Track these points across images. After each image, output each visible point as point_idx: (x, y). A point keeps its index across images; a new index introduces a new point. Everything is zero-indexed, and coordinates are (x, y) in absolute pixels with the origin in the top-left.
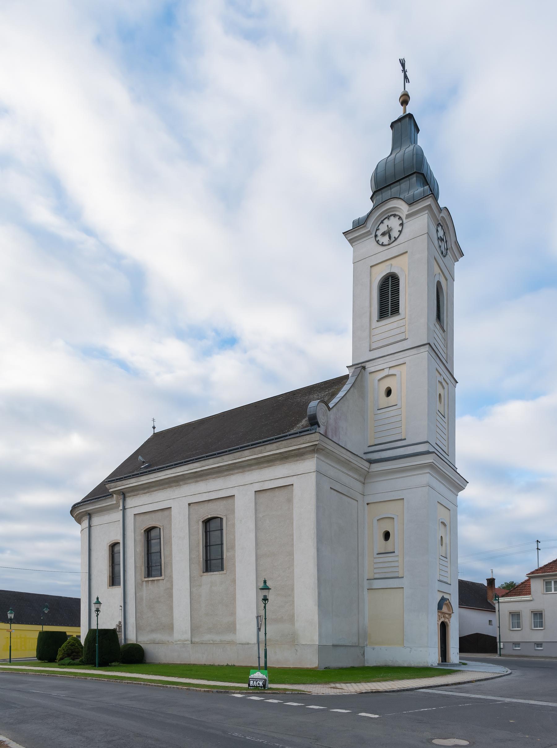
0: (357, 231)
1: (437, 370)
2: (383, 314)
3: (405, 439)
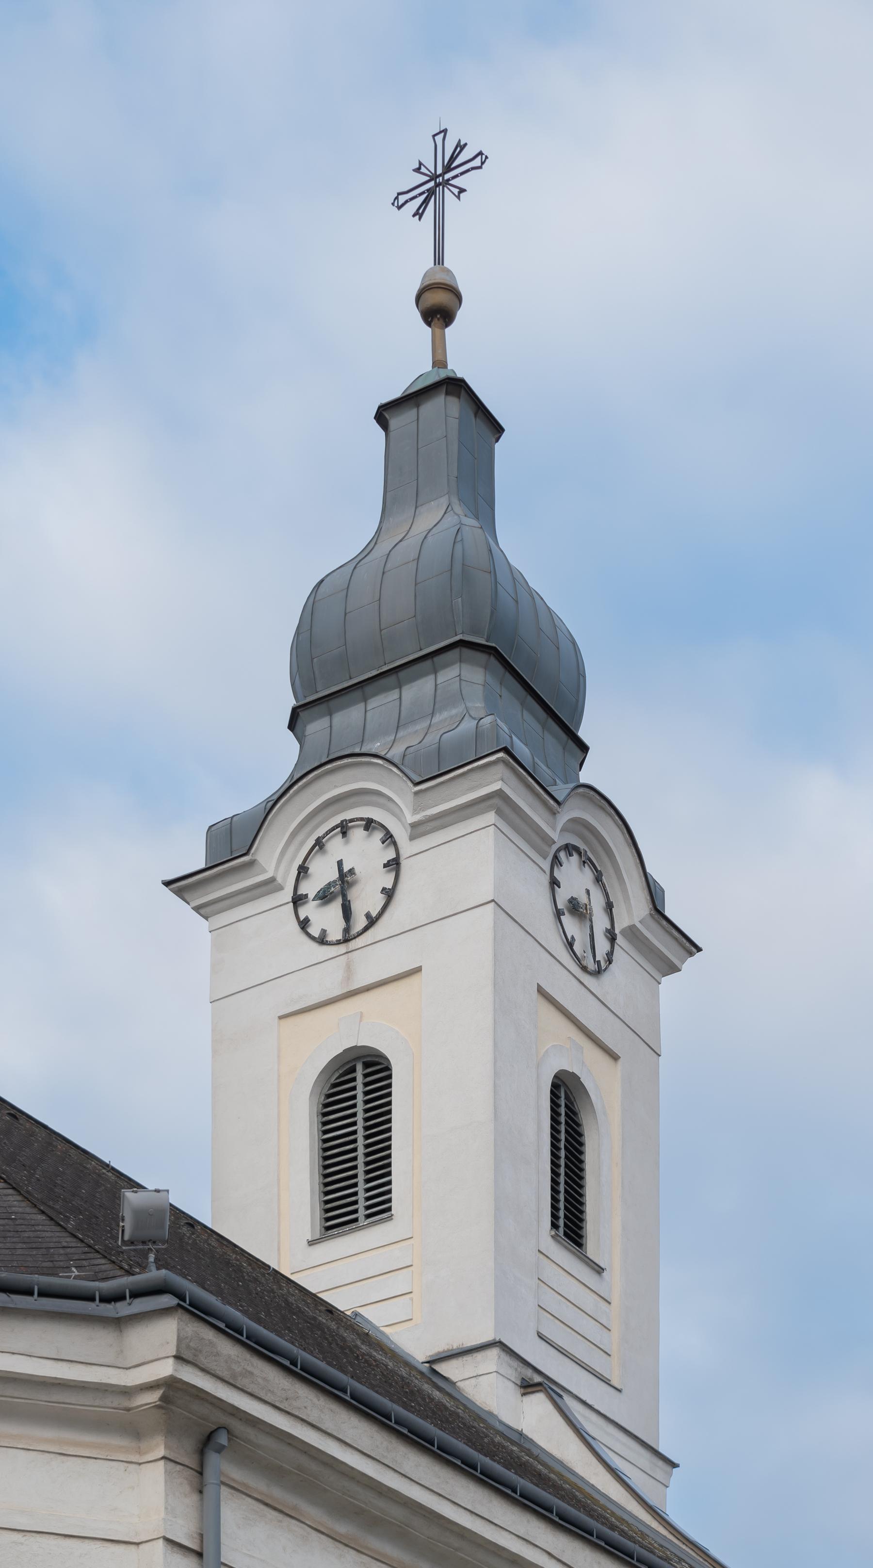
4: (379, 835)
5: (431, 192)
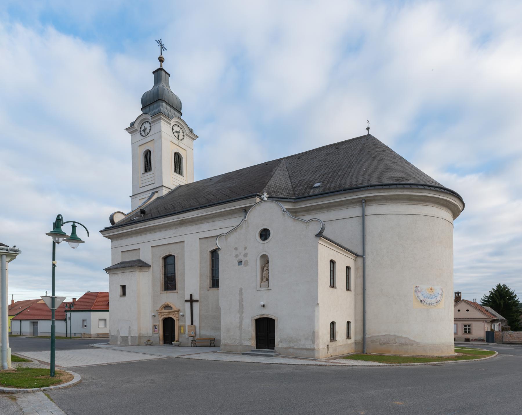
0: (131, 129)
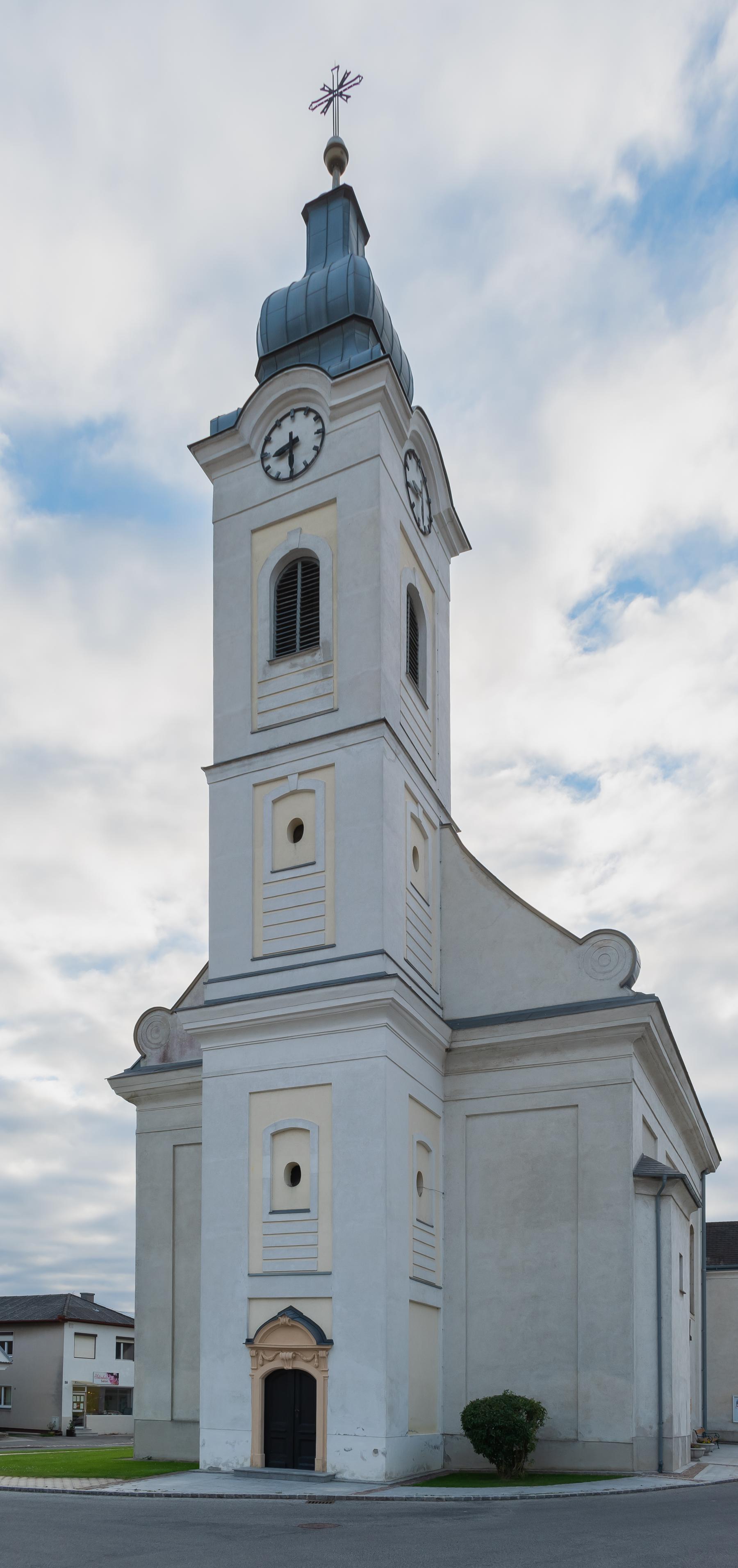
1: (406, 787)
2: (284, 646)
3: (333, 946)
4: (312, 416)
5: (331, 100)
